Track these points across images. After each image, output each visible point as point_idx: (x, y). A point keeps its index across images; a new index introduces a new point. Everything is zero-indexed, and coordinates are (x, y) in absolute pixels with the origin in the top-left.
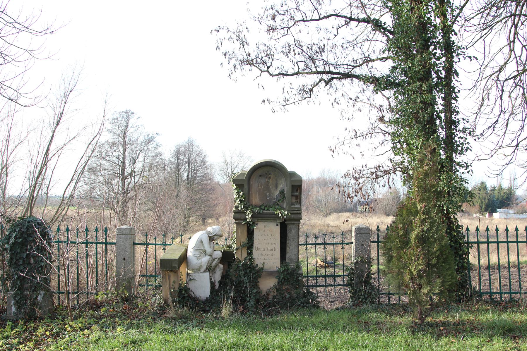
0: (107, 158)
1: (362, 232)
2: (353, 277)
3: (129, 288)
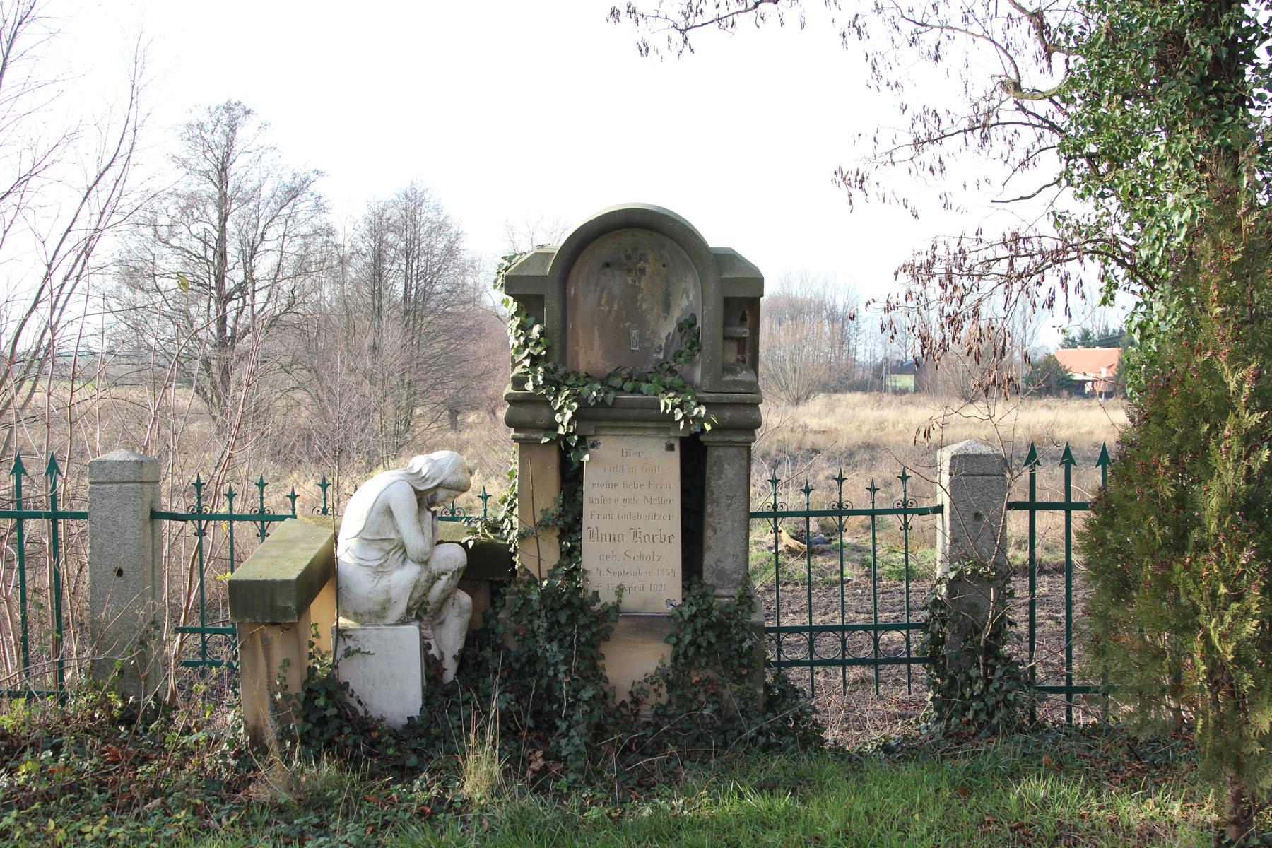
1: (976, 470)
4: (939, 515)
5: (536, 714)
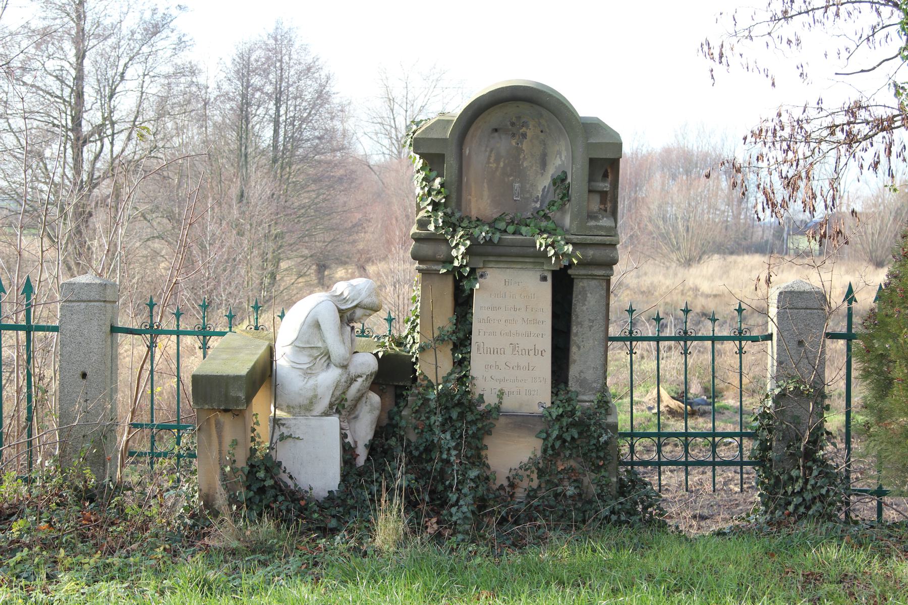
0: (28, 78)
1: (800, 305)
2: (771, 440)
3: (99, 461)
4: (769, 342)
5: (432, 492)
